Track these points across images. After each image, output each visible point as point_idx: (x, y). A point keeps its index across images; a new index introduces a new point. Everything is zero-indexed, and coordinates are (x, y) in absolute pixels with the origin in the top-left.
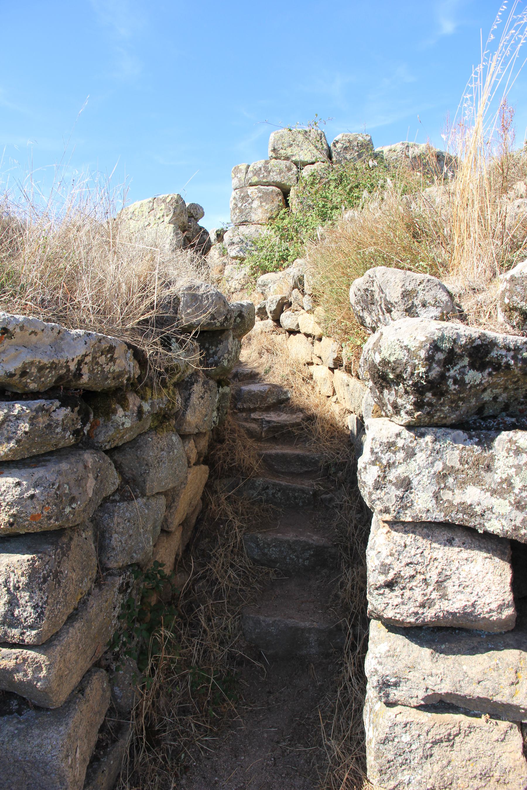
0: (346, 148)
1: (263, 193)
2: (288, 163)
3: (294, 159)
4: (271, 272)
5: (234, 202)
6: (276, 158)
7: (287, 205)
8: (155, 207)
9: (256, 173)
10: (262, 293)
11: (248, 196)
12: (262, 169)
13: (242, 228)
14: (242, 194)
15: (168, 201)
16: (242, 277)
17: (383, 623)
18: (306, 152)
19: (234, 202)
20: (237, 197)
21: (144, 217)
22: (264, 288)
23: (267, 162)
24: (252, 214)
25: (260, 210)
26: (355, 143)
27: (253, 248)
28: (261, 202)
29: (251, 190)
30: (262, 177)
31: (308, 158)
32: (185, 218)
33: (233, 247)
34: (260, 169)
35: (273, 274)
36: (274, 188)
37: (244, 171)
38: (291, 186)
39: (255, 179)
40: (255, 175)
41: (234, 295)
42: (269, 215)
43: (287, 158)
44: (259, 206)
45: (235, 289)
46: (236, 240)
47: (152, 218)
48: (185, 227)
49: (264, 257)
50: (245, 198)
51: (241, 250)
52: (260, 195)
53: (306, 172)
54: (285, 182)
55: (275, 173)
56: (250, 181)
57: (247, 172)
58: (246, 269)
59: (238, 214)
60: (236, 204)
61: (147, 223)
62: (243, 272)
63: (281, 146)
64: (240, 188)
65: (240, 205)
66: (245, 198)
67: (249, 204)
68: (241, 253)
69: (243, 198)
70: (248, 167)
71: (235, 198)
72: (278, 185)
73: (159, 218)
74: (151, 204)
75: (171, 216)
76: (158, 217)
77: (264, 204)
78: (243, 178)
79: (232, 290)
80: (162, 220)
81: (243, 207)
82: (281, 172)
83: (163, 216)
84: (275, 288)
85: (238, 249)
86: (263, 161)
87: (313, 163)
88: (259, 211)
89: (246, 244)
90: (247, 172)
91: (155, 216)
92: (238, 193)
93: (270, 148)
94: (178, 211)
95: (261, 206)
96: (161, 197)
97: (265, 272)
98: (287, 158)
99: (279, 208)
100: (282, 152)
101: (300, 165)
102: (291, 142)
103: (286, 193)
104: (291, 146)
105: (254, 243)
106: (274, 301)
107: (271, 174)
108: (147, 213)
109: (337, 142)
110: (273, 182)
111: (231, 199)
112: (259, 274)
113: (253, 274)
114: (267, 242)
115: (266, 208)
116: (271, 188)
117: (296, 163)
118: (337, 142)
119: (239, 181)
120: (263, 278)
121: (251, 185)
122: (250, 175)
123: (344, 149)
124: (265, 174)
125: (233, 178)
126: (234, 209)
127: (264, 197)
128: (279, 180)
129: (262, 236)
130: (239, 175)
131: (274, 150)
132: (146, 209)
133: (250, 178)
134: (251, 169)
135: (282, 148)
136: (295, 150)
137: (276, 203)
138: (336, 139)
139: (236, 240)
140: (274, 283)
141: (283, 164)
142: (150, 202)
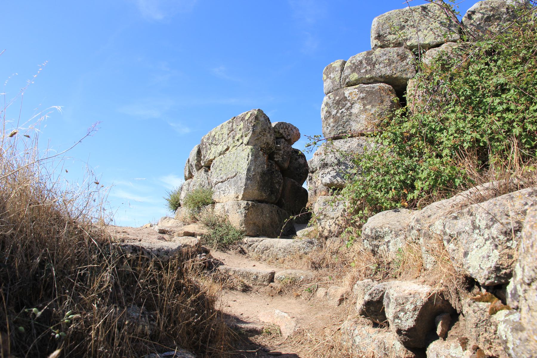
0: (488, 19)
1: (367, 92)
2: (400, 50)
3: (408, 43)
4: (386, 209)
5: (326, 109)
6: (381, 47)
7: (403, 102)
8: (234, 127)
9: (356, 68)
10: (374, 253)
11: (345, 99)
12: (364, 62)
13: (337, 144)
14: (337, 98)
15: (247, 118)
16: (339, 214)
17: (449, 329)
18: (425, 32)
19: (326, 109)
20: (330, 102)
21: (224, 140)
22: (376, 242)
23: (369, 53)
24: (352, 123)
25: (363, 116)
26: (504, 10)
27: (355, 171)
28: (364, 105)
29: (348, 92)
30: (365, 72)
31: (430, 39)
32: (269, 138)
33: (327, 171)
34: (361, 62)
35: (390, 214)
36: (382, 84)
37: (339, 69)
38: (407, 79)
39: (355, 76)
40: (353, 71)
41: (328, 242)
42: (377, 121)
43: (398, 45)
44: (361, 111)
45: (330, 231)
46: (330, 159)
47: (230, 140)
48: (271, 149)
49: (373, 183)
50: (341, 102)
51: (338, 174)
52: (362, 95)
53: (429, 58)
54: (398, 74)
55: (381, 65)
56: (347, 80)
57: (342, 70)
58: (345, 202)
59: (332, 124)
60: (329, 112)
61: (225, 147)
62: (341, 206)
63: (388, 31)
64: (335, 90)
65: (334, 112)
66: (341, 102)
67: (347, 109)
68: (338, 178)
69: (338, 103)
70: (344, 63)
71: (327, 104)
72: (387, 80)
73: (238, 140)
74: (231, 124)
75: (250, 135)
76: (236, 138)
77: (369, 107)
78: (337, 79)
79: (326, 233)
80: (241, 141)
81: (338, 115)
82: (390, 62)
83: (242, 136)
84: (400, 245)
85: (333, 173)
86: (364, 53)
87: (438, 45)
88: (362, 118)
89: (345, 164)
90: (342, 70)
91: (233, 138)
92: (332, 96)
93: (373, 35)
94: (259, 129)
95: (365, 110)
96: (240, 115)
97: (377, 209)
98: (398, 45)
99: (393, 106)
100: (391, 37)
101: (418, 51)
102: (403, 24)
103: (399, 88)
104: (402, 28)
105: (356, 162)
106: (409, 307)
107: (377, 66)
108: (226, 136)
109: (473, 12)
110: (381, 77)
111: (323, 106)
112: (366, 211)
113: (357, 212)
114: (377, 159)
115: (373, 112)
116: (377, 86)
117: (411, 48)
118: (473, 12)
119: (333, 82)
120: (376, 221)
121: (349, 85)
122: (347, 72)
123: (486, 21)
124: (369, 68)
125: (325, 80)
126: (326, 118)
127: (368, 98)
128: (389, 73)
129: (369, 153)
130: (332, 75)
131: (379, 37)
132: (225, 131)
133: (347, 77)
134: (348, 64)
135: (390, 33)
136: (410, 32)
137: (387, 104)
138: (472, 9)
139: (330, 159)
140: (397, 235)
141: (393, 52)
142: (229, 122)
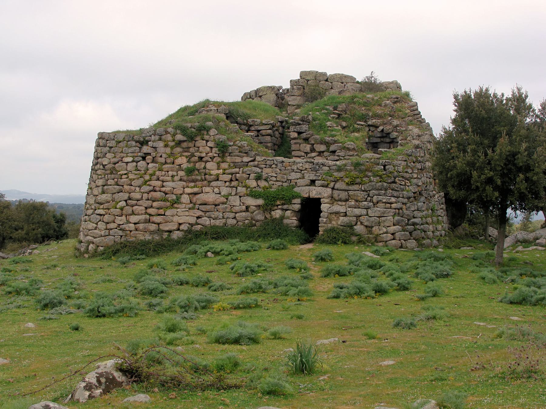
29: (295, 87)
